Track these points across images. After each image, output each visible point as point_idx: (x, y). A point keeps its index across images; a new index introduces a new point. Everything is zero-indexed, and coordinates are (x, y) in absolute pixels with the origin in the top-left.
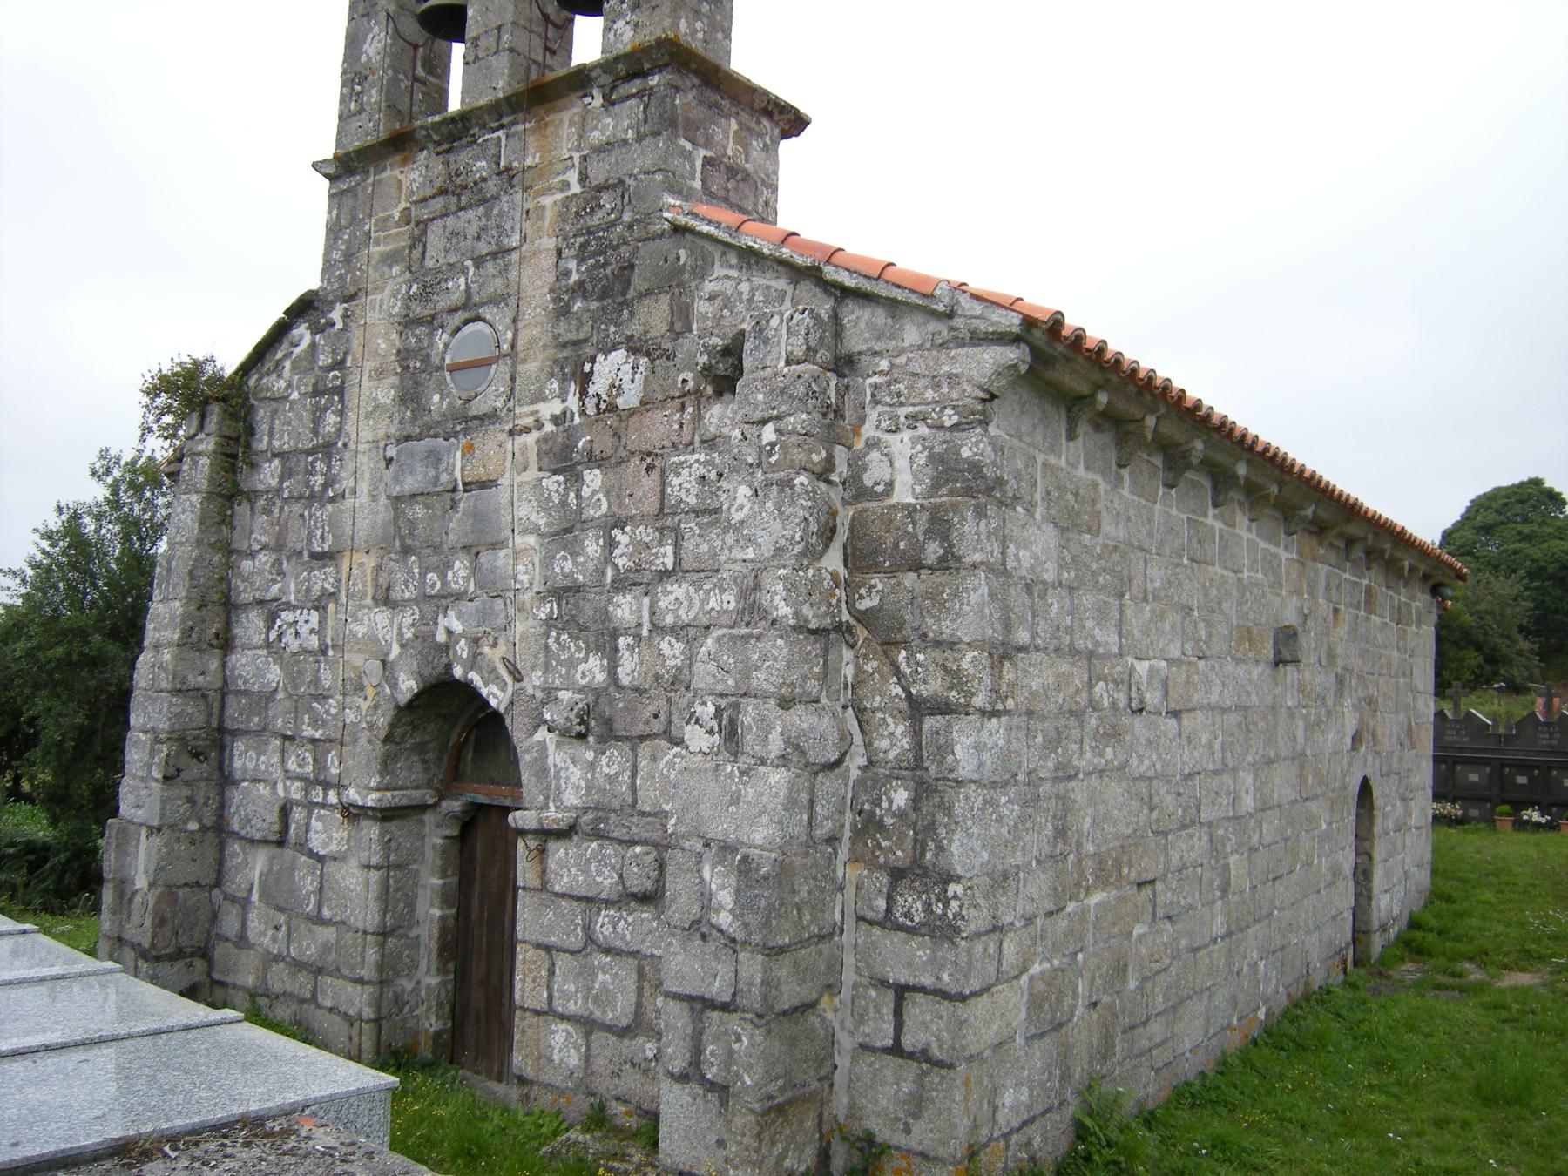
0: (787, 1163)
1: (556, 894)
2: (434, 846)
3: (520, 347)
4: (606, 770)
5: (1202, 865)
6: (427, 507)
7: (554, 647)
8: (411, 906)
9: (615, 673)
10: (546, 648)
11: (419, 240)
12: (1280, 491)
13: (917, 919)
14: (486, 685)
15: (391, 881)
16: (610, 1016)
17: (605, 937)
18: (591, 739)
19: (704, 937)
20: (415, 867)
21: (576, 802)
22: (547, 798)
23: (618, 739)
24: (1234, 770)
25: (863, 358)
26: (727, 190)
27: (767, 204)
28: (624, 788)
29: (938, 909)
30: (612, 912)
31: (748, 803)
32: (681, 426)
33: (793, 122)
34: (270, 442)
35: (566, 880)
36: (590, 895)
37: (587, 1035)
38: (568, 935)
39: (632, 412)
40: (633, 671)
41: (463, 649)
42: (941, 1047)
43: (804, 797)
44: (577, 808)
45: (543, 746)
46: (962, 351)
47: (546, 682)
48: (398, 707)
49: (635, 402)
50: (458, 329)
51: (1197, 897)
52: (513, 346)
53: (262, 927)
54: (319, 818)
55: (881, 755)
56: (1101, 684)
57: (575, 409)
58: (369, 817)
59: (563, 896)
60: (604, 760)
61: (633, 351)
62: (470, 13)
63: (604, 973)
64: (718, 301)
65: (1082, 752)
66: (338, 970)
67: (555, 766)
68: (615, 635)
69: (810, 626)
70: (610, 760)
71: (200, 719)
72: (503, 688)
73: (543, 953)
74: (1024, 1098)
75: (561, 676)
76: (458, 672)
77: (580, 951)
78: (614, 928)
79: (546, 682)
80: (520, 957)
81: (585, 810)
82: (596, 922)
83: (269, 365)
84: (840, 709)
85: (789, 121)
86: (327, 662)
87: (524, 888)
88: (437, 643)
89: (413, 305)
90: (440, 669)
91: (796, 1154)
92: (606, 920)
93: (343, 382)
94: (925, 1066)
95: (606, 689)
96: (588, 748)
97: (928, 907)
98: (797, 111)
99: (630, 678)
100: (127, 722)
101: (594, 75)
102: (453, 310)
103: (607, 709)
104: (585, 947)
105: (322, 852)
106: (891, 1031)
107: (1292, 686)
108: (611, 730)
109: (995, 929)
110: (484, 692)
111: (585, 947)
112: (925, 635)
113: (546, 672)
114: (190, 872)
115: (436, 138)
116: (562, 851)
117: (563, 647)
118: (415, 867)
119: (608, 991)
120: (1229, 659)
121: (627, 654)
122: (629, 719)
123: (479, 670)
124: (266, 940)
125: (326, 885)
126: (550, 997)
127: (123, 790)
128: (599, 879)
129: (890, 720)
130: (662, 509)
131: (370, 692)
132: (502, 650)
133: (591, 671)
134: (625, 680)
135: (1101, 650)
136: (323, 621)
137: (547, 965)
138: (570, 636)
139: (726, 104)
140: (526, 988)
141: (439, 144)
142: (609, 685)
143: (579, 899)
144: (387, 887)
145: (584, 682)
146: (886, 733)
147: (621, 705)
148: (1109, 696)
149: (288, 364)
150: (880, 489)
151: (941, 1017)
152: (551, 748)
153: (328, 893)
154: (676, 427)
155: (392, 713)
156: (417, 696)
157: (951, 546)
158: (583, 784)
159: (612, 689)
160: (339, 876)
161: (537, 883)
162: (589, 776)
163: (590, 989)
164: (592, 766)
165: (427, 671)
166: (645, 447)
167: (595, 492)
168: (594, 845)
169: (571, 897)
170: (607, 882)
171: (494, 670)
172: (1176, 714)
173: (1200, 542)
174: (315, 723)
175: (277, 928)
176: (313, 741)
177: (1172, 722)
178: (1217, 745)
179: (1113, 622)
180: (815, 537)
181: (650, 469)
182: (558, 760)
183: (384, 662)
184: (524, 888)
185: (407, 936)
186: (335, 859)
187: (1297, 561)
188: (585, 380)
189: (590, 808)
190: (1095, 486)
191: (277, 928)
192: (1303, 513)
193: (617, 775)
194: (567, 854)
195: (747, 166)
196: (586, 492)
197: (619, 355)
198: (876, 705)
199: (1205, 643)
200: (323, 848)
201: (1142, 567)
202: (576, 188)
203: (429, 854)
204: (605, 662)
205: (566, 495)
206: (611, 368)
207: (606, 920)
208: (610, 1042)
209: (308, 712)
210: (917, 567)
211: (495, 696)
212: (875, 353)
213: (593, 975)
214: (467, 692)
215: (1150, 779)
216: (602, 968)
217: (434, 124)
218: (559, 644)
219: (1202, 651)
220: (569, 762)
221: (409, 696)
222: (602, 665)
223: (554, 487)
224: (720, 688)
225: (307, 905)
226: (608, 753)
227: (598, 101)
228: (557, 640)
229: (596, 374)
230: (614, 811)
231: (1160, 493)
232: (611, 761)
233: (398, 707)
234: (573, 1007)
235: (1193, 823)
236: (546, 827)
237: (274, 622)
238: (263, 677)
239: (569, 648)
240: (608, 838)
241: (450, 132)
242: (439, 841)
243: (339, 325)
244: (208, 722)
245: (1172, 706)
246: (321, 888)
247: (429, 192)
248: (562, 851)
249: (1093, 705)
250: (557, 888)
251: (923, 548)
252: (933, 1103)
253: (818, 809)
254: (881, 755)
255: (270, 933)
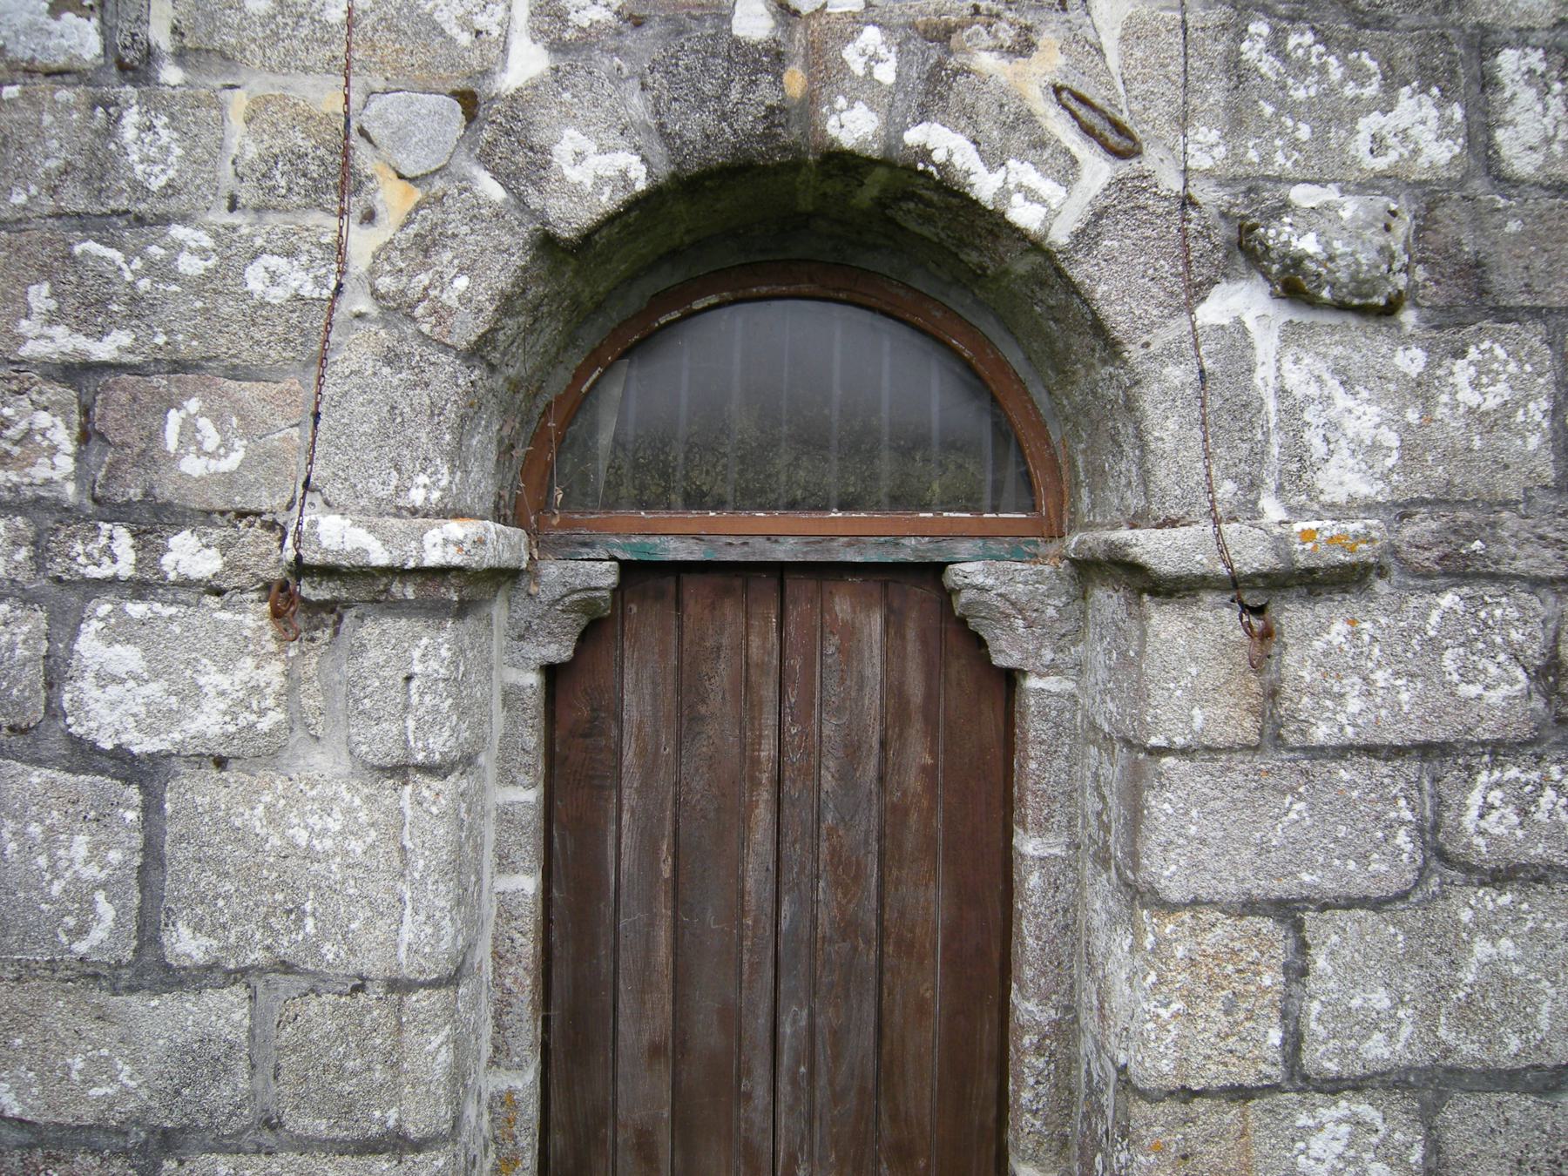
1: (1317, 752)
4: (1468, 397)
7: (1268, 66)
9: (1490, 144)
10: (1236, 69)
14: (994, 160)
16: (1514, 1044)
17: (1494, 841)
18: (1409, 317)
21: (1364, 489)
22: (1254, 485)
23: (1504, 314)
28: (1534, 441)
30: (1513, 772)
35: (1354, 705)
36: (1439, 734)
37: (1427, 1117)
38: (1363, 859)
40: (1548, 141)
44: (1370, 507)
45: (1237, 337)
47: (1238, 160)
48: (547, 244)
54: (120, 632)
58: (397, 608)
59: (1342, 752)
60: (1462, 372)
63: (1493, 938)
66: (271, 1124)
67: (1282, 393)
68: (1484, 43)
70: (1482, 368)
72: (1068, 170)
73: (1267, 925)
75: (1295, 145)
77: (1403, 896)
78: (1523, 812)
79: (1236, 158)
81: (1403, 511)
82: (1462, 807)
86: (151, 103)
88: (736, 42)
92: (1495, 796)
95: (1460, 184)
96: (1406, 341)
99: (1538, 158)
103: (1466, 237)
104: (1420, 882)
105: (143, 745)
108: (1483, 293)
110: (985, 186)
111: (1420, 882)
116: (1339, 628)
119: (1506, 982)
121: (1528, 95)
122: (1540, 264)
123: (966, 119)
125: (178, 854)
128: (1473, 690)
132: (1049, 62)
133: (1404, 135)
134: (1523, 164)
137: (1281, 950)
138: (1323, 38)
142: (1468, 175)
143: (1395, 752)
144: (968, 365)
145: (1381, 164)
147: (1513, 226)
152: (1266, 344)
158: (1391, 439)
159: (1479, 186)
160: (254, 818)
161: (1247, 729)
162: (1412, 416)
163: (1442, 989)
164: (1422, 389)
165: (693, 124)
168: (1449, 600)
169: (1371, 750)
170: (1495, 697)
171: (1027, 119)
176: (75, 372)
182: (1295, 379)
183: (469, 101)
186: (221, 763)
189: (1423, 502)
193: (1507, 409)
194: (1356, 634)
200: (152, 731)
204: (1457, 112)
207: (1495, 796)
208: (1512, 1114)
209: (46, 272)
211: (1031, 195)
213: (1453, 950)
216: (1487, 927)
218: (1284, 56)
220: (1333, 383)
222: (1445, 122)
225: (81, 931)
226: (1473, 354)
228: (1276, 45)
230: (1506, 504)
232: (1484, 374)
233: (547, 244)
236: (1302, 561)
239: (1323, 70)
240: (1494, 577)
248: (1339, 628)
250: (1321, 733)
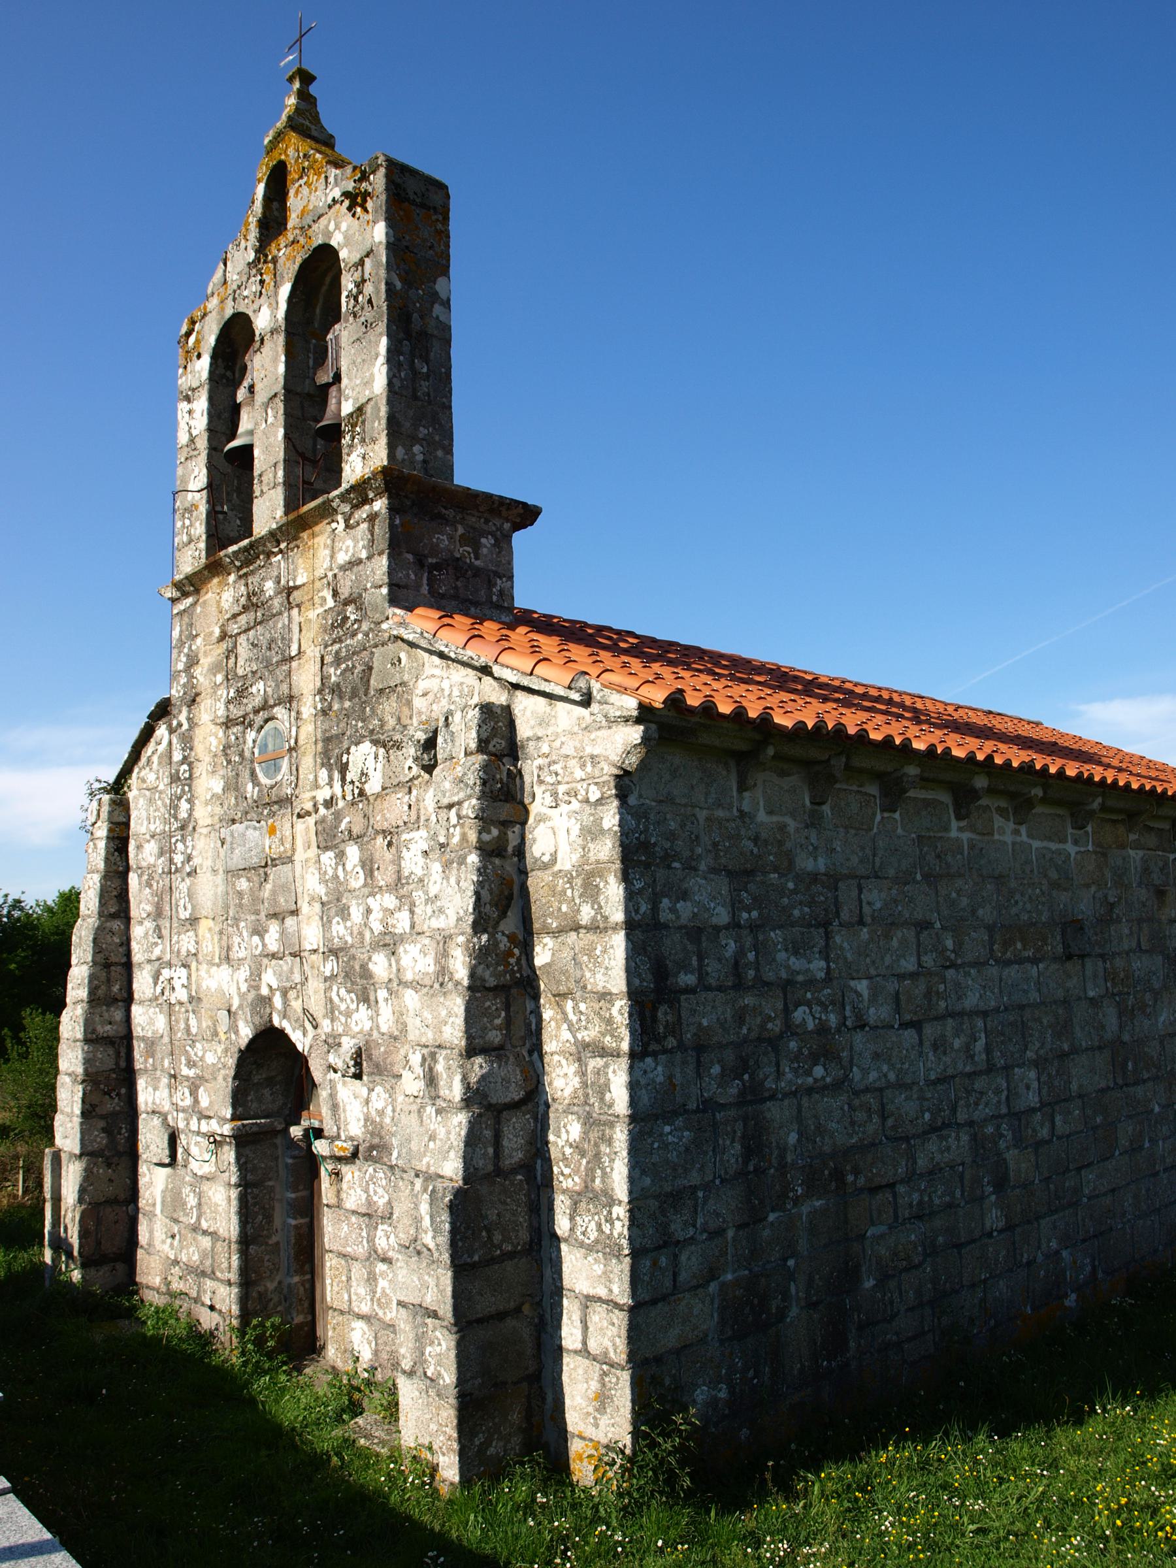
0: (491, 1451)
2: (287, 1164)
3: (301, 742)
5: (963, 1164)
6: (249, 880)
7: (336, 999)
8: (269, 1218)
11: (231, 652)
12: (1045, 792)
13: (592, 1238)
15: (249, 1197)
19: (419, 1253)
20: (270, 1183)
24: (1007, 1068)
25: (531, 743)
26: (456, 588)
27: (501, 593)
29: (606, 1228)
31: (441, 1140)
32: (410, 806)
33: (527, 515)
34: (148, 828)
39: (378, 796)
41: (277, 1001)
42: (615, 1351)
43: (488, 1133)
46: (600, 733)
49: (378, 789)
50: (262, 727)
51: (958, 1193)
52: (296, 742)
53: (164, 1236)
55: (560, 1093)
56: (801, 1009)
57: (339, 794)
59: (354, 1212)
61: (375, 742)
62: (256, 453)
64: (430, 697)
65: (779, 1074)
69: (487, 985)
71: (110, 1064)
74: (723, 1395)
76: (276, 1022)
80: (328, 1264)
83: (143, 760)
84: (526, 1054)
85: (520, 515)
87: (327, 1206)
89: (231, 707)
90: (266, 1018)
91: (501, 1444)
93: (191, 775)
94: (605, 1367)
97: (599, 1226)
98: (524, 504)
100: (57, 1068)
101: (334, 504)
102: (256, 711)
106: (580, 1337)
107: (1095, 976)
109: (665, 1245)
112: (585, 987)
113: (332, 1021)
114: (110, 1191)
115: (238, 563)
117: (342, 1000)
118: (270, 1183)
120: (992, 962)
124: (166, 1247)
126: (350, 1301)
127: (56, 1124)
129: (564, 1062)
130: (399, 879)
131: (223, 1037)
135: (800, 978)
136: (189, 977)
139: (450, 513)
140: (332, 1289)
141: (239, 569)
144: (247, 1201)
146: (562, 1074)
148: (814, 1018)
149: (155, 759)
150: (546, 859)
151: (613, 1324)
153: (205, 1208)
154: (406, 808)
155: (236, 1056)
156: (252, 1042)
157: (600, 907)
160: (210, 1193)
166: (386, 825)
167: (355, 866)
172: (917, 1025)
173: (938, 856)
174: (191, 1064)
175: (173, 1237)
177: (910, 1035)
178: (980, 1044)
179: (816, 950)
180: (488, 906)
181: (390, 844)
183: (229, 1011)
184: (327, 1206)
185: (267, 1244)
186: (208, 1179)
187: (1095, 852)
188: (344, 769)
190: (782, 828)
191: (173, 1237)
192: (1088, 808)
195: (477, 563)
196: (349, 867)
197: (366, 747)
198: (554, 1049)
199: (953, 951)
201: (855, 893)
202: (330, 603)
203: (283, 1173)
205: (336, 869)
206: (362, 756)
210: (577, 928)
212: (539, 738)
214: (281, 1034)
215: (881, 1090)
217: (234, 552)
219: (948, 959)
221: (246, 1041)
223: (328, 862)
224: (424, 1040)
227: (342, 525)
229: (351, 764)
231: (878, 818)
233: (240, 1051)
234: (365, 1308)
235: (945, 1126)
237: (158, 979)
238: (153, 1024)
241: (246, 559)
242: (290, 1161)
243: (185, 726)
244: (117, 1064)
245: (908, 1017)
246: (200, 1204)
247: (237, 609)
249: (790, 1029)
251: (578, 911)
252: (612, 1401)
253: (505, 1143)
254: (560, 1093)
255: (169, 1240)
